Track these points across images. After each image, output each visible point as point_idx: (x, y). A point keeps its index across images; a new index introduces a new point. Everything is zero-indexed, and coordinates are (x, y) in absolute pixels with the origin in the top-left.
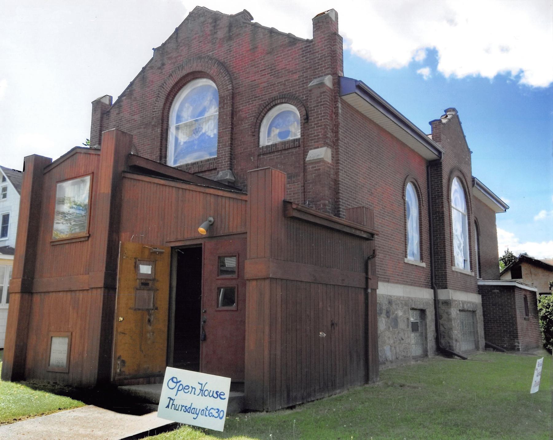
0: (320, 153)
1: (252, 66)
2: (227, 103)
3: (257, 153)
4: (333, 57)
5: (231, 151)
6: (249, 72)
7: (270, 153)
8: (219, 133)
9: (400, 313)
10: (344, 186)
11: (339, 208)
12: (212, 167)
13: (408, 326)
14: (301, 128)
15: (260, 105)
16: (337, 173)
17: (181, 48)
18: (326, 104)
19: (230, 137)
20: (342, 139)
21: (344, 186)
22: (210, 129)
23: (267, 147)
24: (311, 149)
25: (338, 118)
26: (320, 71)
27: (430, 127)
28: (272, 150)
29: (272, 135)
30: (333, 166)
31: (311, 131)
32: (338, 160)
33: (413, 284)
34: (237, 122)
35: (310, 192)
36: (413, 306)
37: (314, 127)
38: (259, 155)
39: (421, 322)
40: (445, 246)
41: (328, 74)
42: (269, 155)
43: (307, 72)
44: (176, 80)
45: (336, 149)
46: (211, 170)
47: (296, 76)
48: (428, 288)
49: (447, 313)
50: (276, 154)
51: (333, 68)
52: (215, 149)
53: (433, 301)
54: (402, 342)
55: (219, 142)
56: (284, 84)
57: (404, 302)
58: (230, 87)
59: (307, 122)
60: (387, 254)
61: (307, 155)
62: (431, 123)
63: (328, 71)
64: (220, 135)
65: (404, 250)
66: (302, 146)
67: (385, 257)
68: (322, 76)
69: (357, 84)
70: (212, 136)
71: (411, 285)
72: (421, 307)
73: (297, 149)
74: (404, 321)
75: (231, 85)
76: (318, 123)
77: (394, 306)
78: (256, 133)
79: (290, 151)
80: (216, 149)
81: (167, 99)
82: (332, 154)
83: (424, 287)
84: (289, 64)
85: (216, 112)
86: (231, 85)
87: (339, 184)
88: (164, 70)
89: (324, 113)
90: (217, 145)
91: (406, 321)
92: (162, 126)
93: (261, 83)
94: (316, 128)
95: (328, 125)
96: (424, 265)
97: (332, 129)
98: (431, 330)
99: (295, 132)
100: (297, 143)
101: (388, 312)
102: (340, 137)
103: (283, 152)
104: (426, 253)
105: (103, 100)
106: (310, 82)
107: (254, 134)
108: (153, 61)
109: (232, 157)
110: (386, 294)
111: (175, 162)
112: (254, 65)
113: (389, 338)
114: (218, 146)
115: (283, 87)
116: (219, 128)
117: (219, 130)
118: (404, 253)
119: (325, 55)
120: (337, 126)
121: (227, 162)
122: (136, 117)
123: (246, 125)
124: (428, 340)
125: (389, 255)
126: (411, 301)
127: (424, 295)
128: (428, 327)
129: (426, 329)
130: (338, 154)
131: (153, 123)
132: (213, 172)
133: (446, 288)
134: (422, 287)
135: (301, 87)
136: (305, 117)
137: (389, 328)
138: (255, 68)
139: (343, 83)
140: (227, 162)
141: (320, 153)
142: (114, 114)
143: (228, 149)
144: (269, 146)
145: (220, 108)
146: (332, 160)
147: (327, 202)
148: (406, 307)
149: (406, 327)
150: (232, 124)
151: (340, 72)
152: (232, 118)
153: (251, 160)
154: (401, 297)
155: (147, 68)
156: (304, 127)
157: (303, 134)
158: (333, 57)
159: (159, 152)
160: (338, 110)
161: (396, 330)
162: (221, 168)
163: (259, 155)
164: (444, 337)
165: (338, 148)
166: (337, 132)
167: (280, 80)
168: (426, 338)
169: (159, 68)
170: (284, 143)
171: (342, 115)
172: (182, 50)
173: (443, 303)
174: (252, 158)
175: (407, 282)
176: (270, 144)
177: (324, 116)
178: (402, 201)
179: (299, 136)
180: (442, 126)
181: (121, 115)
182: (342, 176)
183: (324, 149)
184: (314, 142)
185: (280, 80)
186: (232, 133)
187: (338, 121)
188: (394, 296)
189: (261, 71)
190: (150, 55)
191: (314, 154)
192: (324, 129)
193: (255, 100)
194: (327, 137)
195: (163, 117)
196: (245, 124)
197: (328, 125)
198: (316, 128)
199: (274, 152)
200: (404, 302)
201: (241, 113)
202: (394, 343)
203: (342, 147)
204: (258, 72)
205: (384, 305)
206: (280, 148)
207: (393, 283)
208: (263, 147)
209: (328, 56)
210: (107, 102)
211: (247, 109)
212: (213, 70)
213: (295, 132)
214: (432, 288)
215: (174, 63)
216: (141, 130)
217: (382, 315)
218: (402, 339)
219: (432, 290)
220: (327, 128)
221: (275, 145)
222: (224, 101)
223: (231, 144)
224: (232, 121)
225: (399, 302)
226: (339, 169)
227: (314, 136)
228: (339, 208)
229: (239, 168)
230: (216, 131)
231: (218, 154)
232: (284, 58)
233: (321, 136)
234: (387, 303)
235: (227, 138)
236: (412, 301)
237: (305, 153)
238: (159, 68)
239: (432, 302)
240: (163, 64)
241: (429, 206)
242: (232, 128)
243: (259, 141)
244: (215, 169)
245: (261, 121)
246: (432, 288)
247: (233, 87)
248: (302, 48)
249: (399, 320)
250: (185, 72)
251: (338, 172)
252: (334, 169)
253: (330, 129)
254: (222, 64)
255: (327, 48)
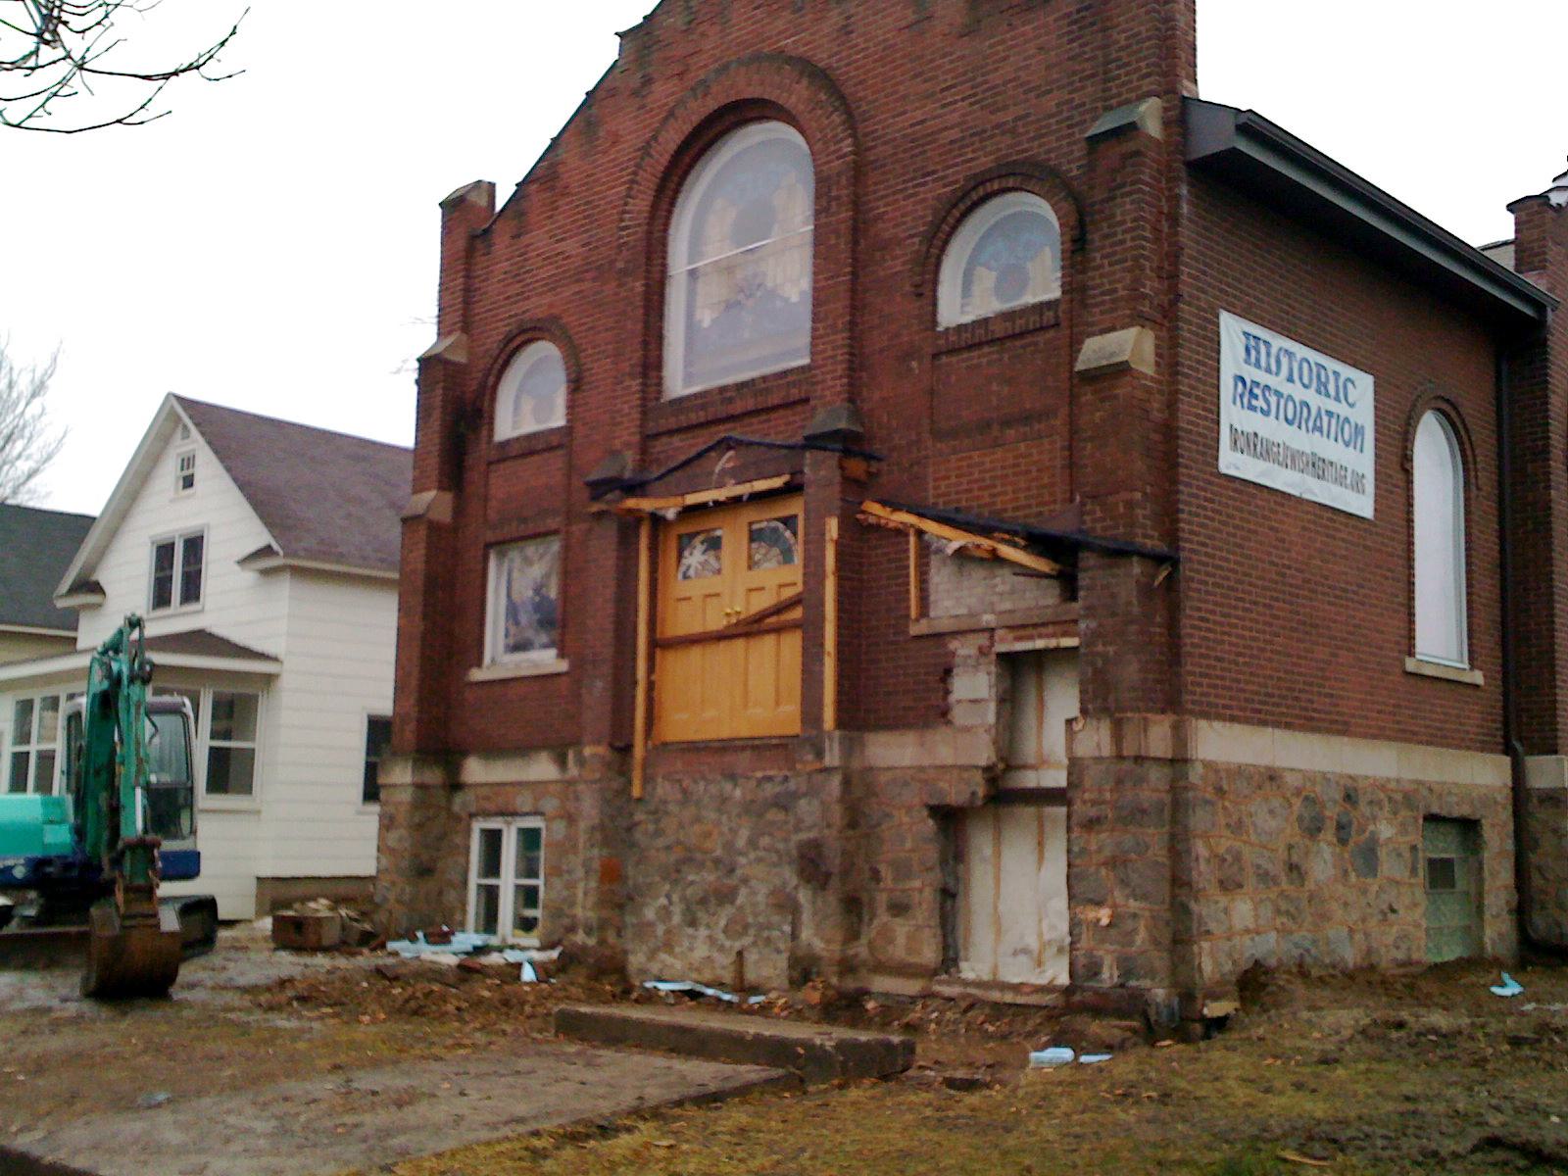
0: (1128, 345)
1: (916, 76)
2: (837, 198)
3: (929, 350)
4: (1166, 38)
5: (851, 346)
6: (904, 97)
7: (970, 347)
8: (815, 290)
9: (1385, 830)
10: (1196, 443)
11: (1178, 511)
12: (795, 394)
13: (1414, 871)
14: (1063, 268)
15: (938, 198)
16: (1172, 405)
17: (701, 29)
18: (1140, 191)
19: (847, 302)
20: (1191, 296)
21: (1196, 443)
22: (791, 275)
23: (961, 328)
24: (1093, 334)
25: (1176, 234)
26: (1124, 84)
27: (1511, 218)
28: (978, 336)
29: (976, 289)
30: (1160, 382)
31: (1093, 279)
32: (1177, 364)
33: (1439, 738)
34: (869, 257)
35: (1086, 466)
36: (1435, 810)
37: (1101, 266)
38: (935, 356)
39: (1465, 860)
40: (1553, 616)
41: (1149, 94)
42: (965, 355)
43: (1083, 88)
44: (688, 128)
45: (1169, 329)
46: (795, 403)
47: (1050, 103)
48: (1492, 751)
49: (1555, 831)
50: (986, 349)
51: (1164, 74)
52: (804, 340)
53: (1507, 792)
54: (1392, 917)
55: (816, 318)
56: (1013, 131)
57: (1399, 797)
58: (847, 146)
59: (1082, 249)
60: (1341, 648)
61: (1079, 351)
62: (1511, 207)
63: (1147, 85)
64: (820, 299)
65: (1404, 632)
66: (1064, 324)
67: (1336, 655)
68: (1128, 102)
69: (1242, 119)
70: (795, 298)
71: (1429, 743)
72: (1464, 811)
73: (1051, 334)
74: (1399, 855)
75: (849, 141)
76: (1115, 253)
77: (1365, 809)
78: (926, 289)
79: (1029, 339)
80: (808, 339)
81: (660, 190)
82: (1157, 347)
83: (1477, 749)
84: (1027, 67)
85: (805, 224)
86: (849, 141)
87: (1178, 437)
88: (649, 99)
89: (1135, 220)
90: (808, 325)
91: (1407, 855)
92: (648, 271)
93: (946, 129)
94: (1107, 269)
95: (1146, 258)
96: (1478, 677)
97: (1160, 268)
98: (1499, 883)
99: (1044, 284)
100: (1049, 315)
101: (1341, 827)
102: (1184, 290)
103: (1008, 344)
104: (1489, 641)
105: (473, 197)
106: (1094, 119)
107: (920, 290)
108: (617, 71)
109: (857, 365)
110: (1338, 769)
111: (689, 378)
112: (920, 74)
113: (1346, 904)
114: (814, 329)
115: (1008, 140)
116: (815, 273)
117: (815, 281)
118: (1404, 641)
119: (1139, 33)
120: (1174, 256)
121: (841, 377)
122: (571, 246)
123: (897, 263)
124: (1487, 916)
125: (1349, 649)
126: (1425, 792)
127: (1478, 776)
128: (1486, 874)
129: (1480, 881)
130: (1178, 345)
131: (620, 265)
132: (799, 408)
133: (1556, 752)
134: (1468, 748)
135: (1063, 137)
136: (1076, 232)
137: (1346, 872)
138: (925, 81)
139: (1196, 118)
140: (841, 377)
141: (1128, 345)
142: (501, 242)
143: (841, 338)
144: (966, 325)
145: (818, 213)
146: (1157, 364)
147: (1138, 495)
148: (1404, 813)
149: (1407, 874)
150: (855, 259)
151: (1186, 83)
152: (856, 243)
153: (910, 370)
154: (1389, 780)
155: (601, 94)
156: (1072, 266)
157: (1068, 288)
158: (1166, 38)
159: (640, 354)
160: (1178, 206)
161: (1369, 880)
162: (822, 397)
163: (935, 356)
164: (1543, 908)
165: (1177, 328)
166: (1174, 277)
167: (1000, 117)
168: (1480, 909)
169: (635, 93)
170: (1008, 316)
171: (1190, 220)
172: (703, 34)
173: (1541, 801)
174: (914, 364)
175: (1414, 733)
176: (967, 319)
177: (1133, 229)
178: (1401, 476)
179: (1055, 293)
180: (1551, 214)
181: (525, 239)
182: (1189, 413)
183: (1133, 332)
184: (1102, 313)
185: (1000, 117)
186: (853, 291)
187: (1176, 243)
188: (1367, 777)
189: (943, 90)
190: (608, 52)
191: (1096, 350)
192: (1129, 270)
193: (924, 184)
194: (1144, 296)
195: (649, 244)
196: (894, 258)
197: (1146, 258)
198: (1107, 269)
199: (980, 345)
200: (1399, 797)
201: (881, 225)
202: (1364, 920)
203: (1190, 323)
204: (933, 94)
205: (1329, 804)
206: (999, 330)
207: (1364, 736)
208: (947, 329)
209: (1149, 38)
210: (483, 202)
211: (902, 214)
212: (796, 94)
213: (1044, 284)
214: (1506, 752)
215: (681, 75)
216: (587, 285)
217: (1321, 836)
218: (1393, 911)
219: (1507, 760)
220: (1142, 269)
221: (984, 322)
222: (830, 190)
223: (852, 324)
224: (853, 251)
225: (1382, 796)
226: (1177, 391)
227: (1103, 294)
228: (1178, 511)
229: (877, 395)
230: (805, 284)
231: (813, 354)
232: (1012, 47)
233: (1122, 293)
234: (1338, 796)
235: (840, 306)
236: (1430, 790)
237: (1075, 345)
238: (635, 93)
239: (1504, 796)
240: (648, 81)
241: (1500, 484)
242: (854, 274)
243: (934, 313)
244: (807, 400)
245: (943, 249)
246: (1508, 749)
247: (856, 144)
248: (1068, 15)
249: (1382, 853)
250: (712, 105)
251: (1177, 401)
252: (1160, 392)
253: (1152, 270)
254: (821, 77)
255: (1147, 13)
